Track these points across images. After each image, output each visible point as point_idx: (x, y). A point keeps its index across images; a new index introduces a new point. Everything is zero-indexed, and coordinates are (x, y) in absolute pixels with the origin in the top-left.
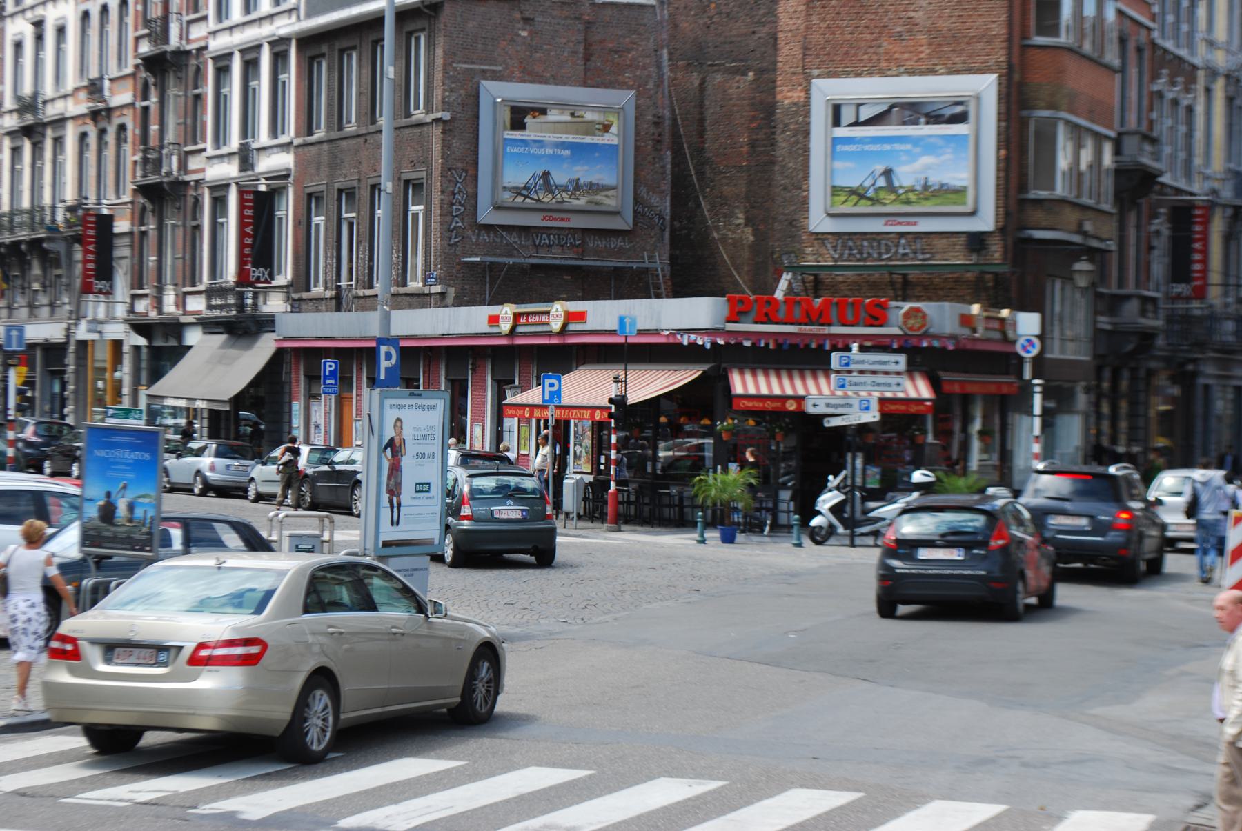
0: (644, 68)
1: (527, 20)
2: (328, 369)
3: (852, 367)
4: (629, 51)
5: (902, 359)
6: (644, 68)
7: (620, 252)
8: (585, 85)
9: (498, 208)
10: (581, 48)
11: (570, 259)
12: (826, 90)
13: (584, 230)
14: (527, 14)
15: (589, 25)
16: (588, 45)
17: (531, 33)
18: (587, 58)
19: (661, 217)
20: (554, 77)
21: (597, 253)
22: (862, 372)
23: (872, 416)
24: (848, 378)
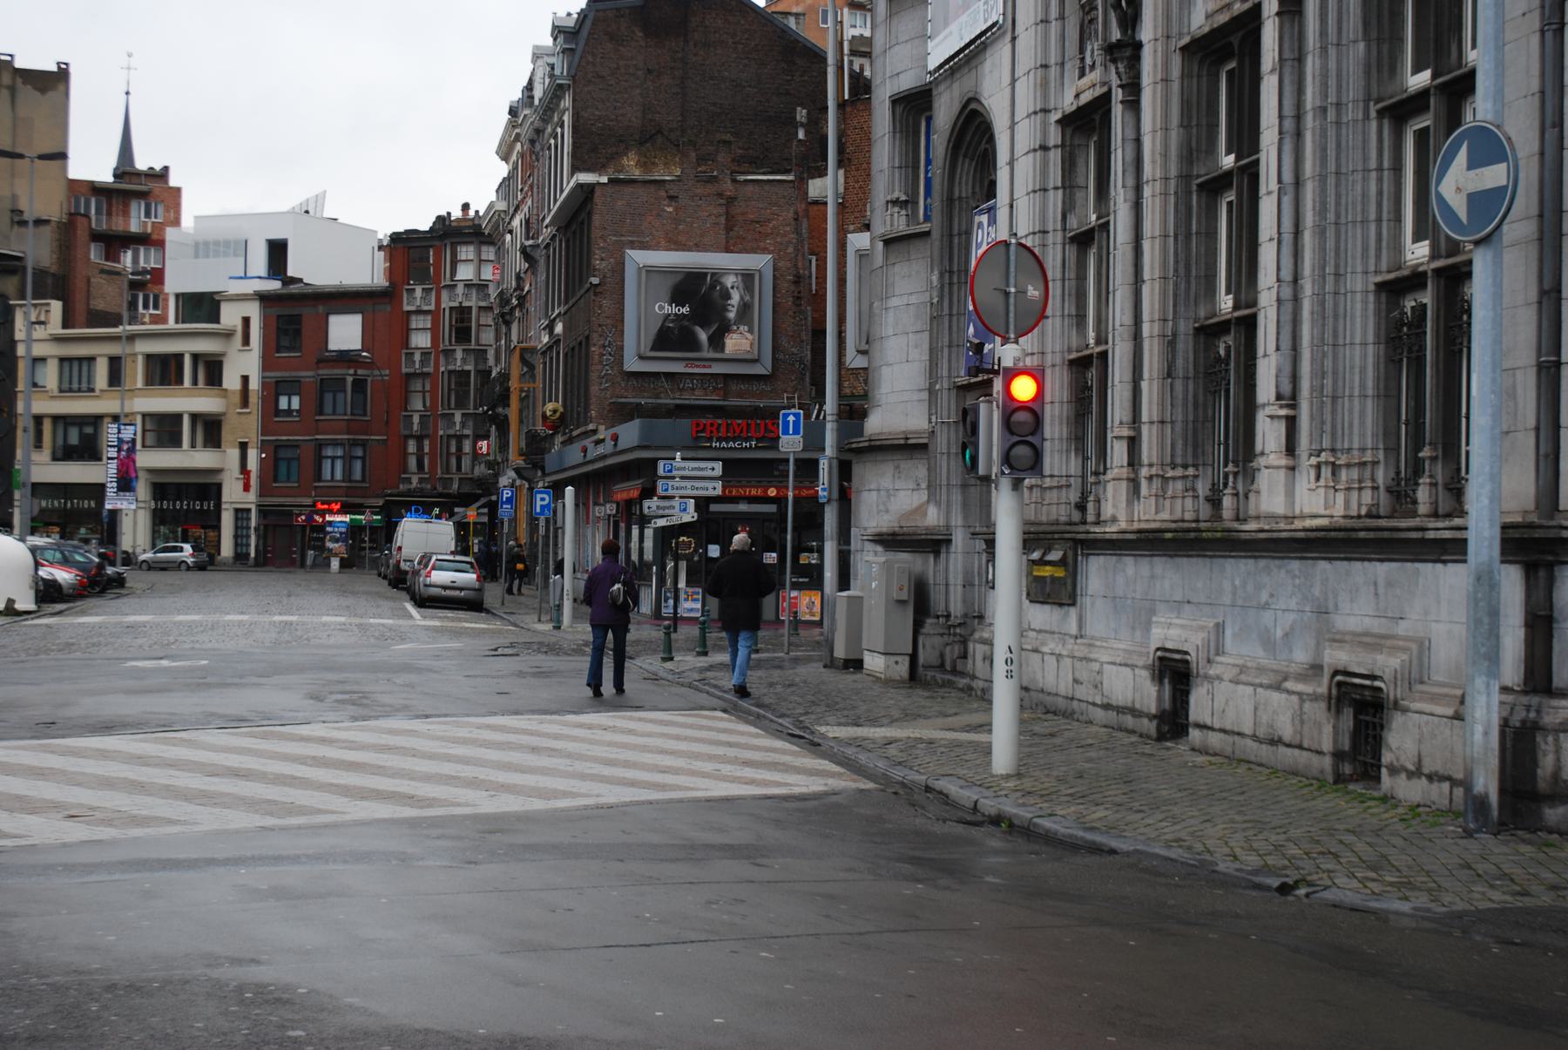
0: (784, 235)
1: (672, 198)
2: (539, 503)
3: (675, 473)
4: (769, 221)
5: (719, 466)
6: (784, 235)
7: (762, 395)
8: (728, 250)
9: (641, 358)
10: (723, 220)
11: (713, 399)
12: (639, 258)
13: (726, 376)
14: (671, 193)
15: (731, 200)
16: (729, 217)
17: (676, 209)
18: (729, 229)
19: (801, 362)
20: (696, 245)
21: (740, 395)
22: (682, 478)
23: (690, 516)
24: (671, 483)
